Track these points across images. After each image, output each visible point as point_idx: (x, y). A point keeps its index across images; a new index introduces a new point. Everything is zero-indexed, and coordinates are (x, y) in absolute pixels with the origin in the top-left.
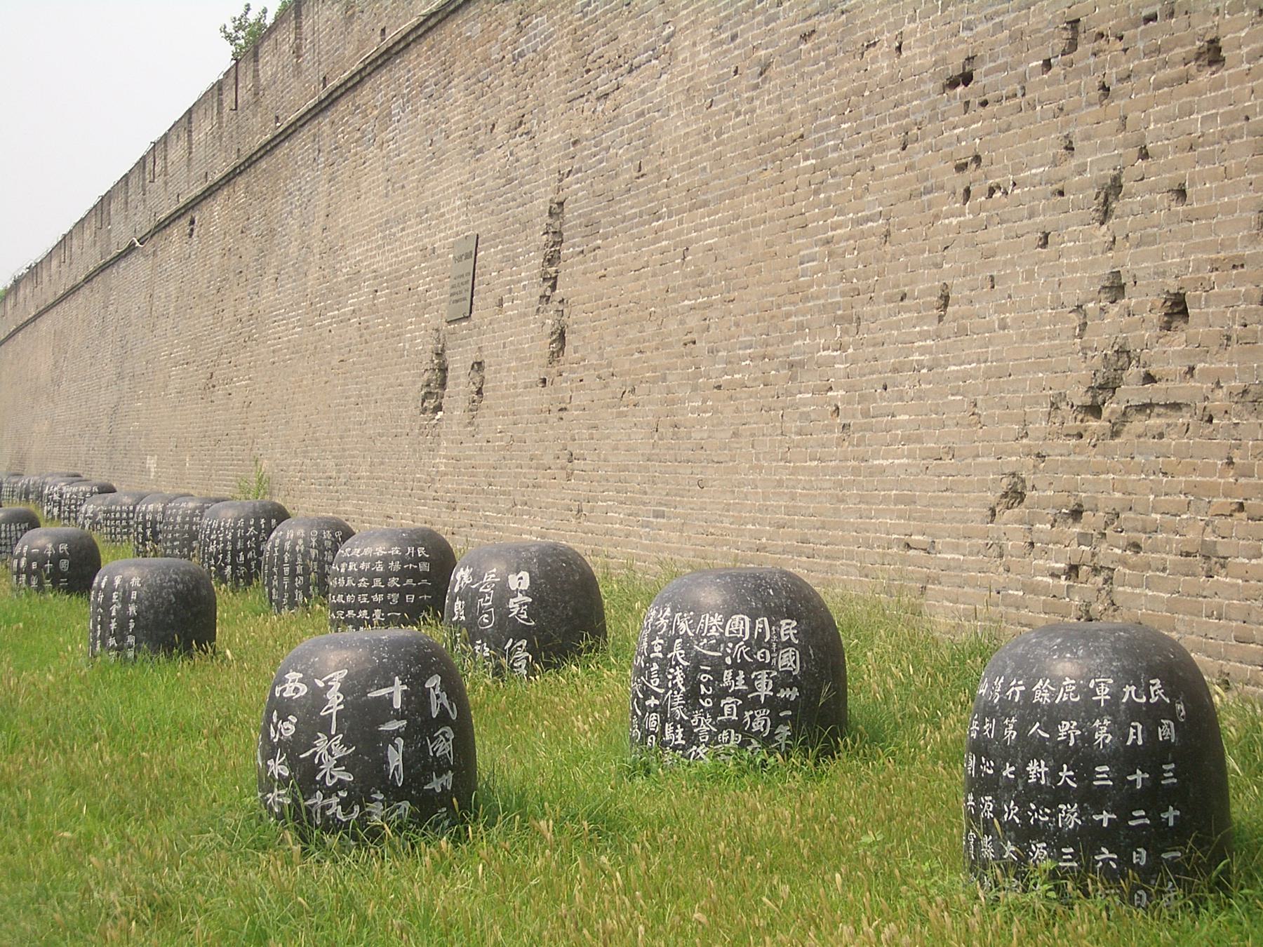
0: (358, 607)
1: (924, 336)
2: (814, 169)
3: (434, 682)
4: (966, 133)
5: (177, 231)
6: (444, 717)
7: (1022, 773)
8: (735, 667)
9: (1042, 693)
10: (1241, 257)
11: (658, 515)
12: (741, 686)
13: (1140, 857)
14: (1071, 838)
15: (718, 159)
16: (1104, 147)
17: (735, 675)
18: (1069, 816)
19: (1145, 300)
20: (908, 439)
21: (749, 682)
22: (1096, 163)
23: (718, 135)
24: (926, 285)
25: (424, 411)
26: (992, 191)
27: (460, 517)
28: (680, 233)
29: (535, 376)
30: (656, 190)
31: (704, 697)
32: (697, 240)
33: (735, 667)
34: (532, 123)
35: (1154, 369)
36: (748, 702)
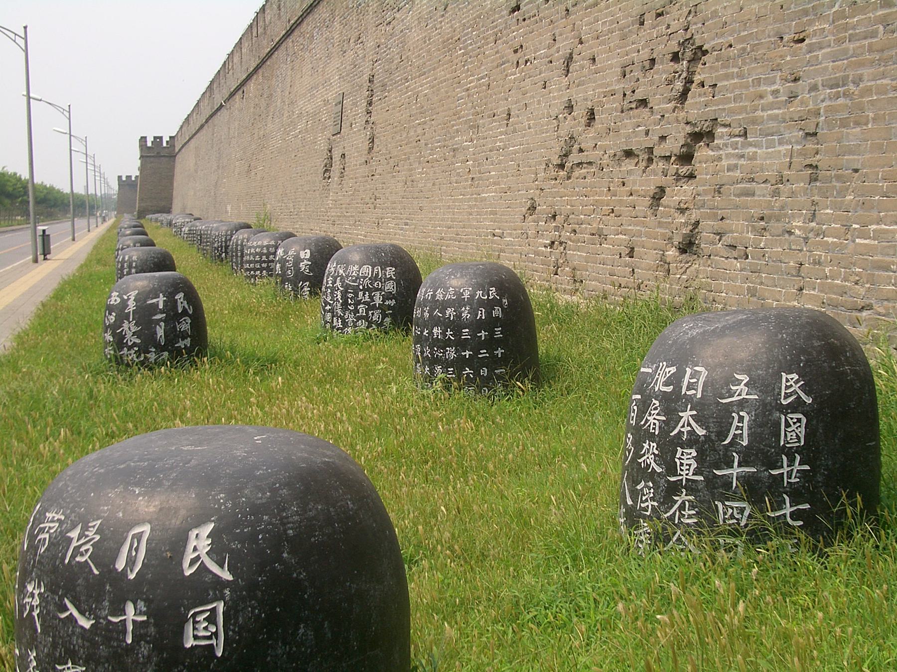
0: (255, 270)
1: (501, 133)
2: (464, 54)
3: (180, 296)
4: (517, 35)
5: (238, 97)
6: (185, 312)
7: (431, 333)
8: (364, 290)
9: (439, 297)
10: (614, 90)
11: (406, 224)
12: (367, 299)
13: (484, 372)
14: (451, 363)
15: (429, 51)
16: (567, 38)
17: (364, 294)
18: (451, 353)
19: (580, 112)
20: (495, 184)
21: (371, 297)
22: (564, 46)
23: (429, 40)
24: (501, 110)
25: (325, 178)
26: (526, 62)
27: (337, 229)
28: (415, 88)
29: (363, 160)
30: (406, 68)
31: (350, 305)
32: (421, 91)
33: (364, 290)
34: (363, 39)
35: (582, 146)
36: (371, 307)
